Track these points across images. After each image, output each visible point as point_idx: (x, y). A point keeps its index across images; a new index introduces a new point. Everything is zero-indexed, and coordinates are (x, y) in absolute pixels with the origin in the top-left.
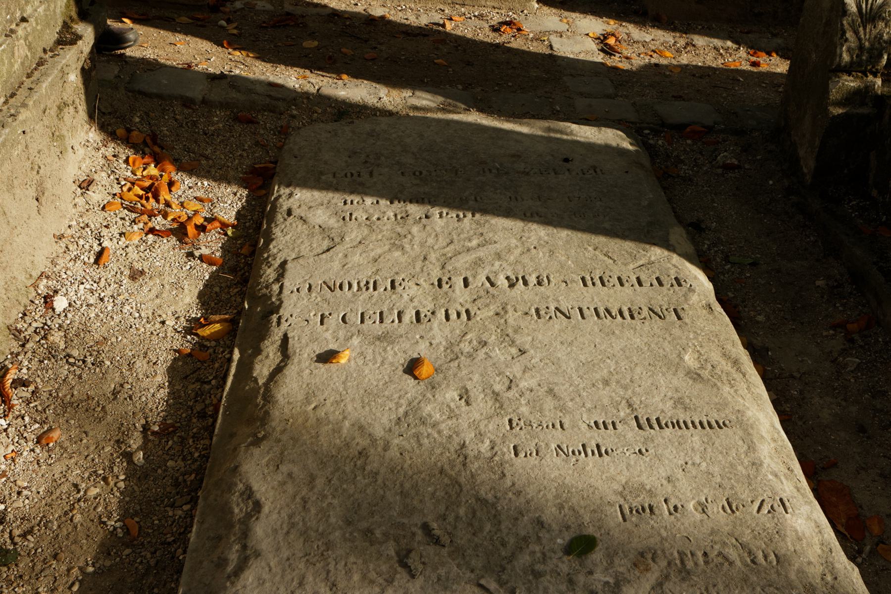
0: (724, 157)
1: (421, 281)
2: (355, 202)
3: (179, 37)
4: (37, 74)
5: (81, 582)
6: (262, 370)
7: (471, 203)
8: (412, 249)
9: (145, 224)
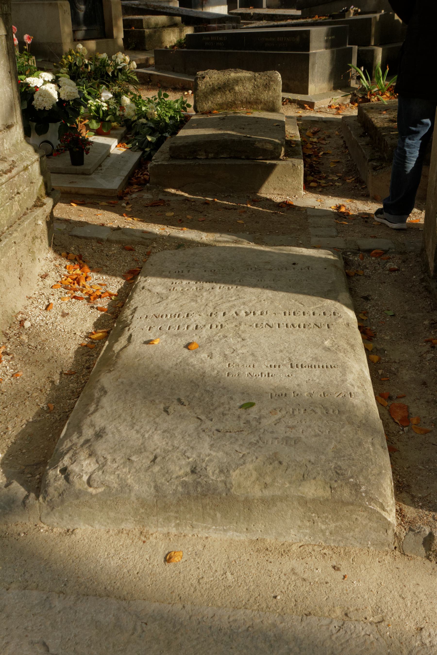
0: (391, 265)
1: (202, 314)
2: (177, 283)
3: (100, 212)
4: (23, 219)
5: (26, 425)
6: (117, 347)
7: (237, 282)
8: (201, 301)
9: (72, 294)
